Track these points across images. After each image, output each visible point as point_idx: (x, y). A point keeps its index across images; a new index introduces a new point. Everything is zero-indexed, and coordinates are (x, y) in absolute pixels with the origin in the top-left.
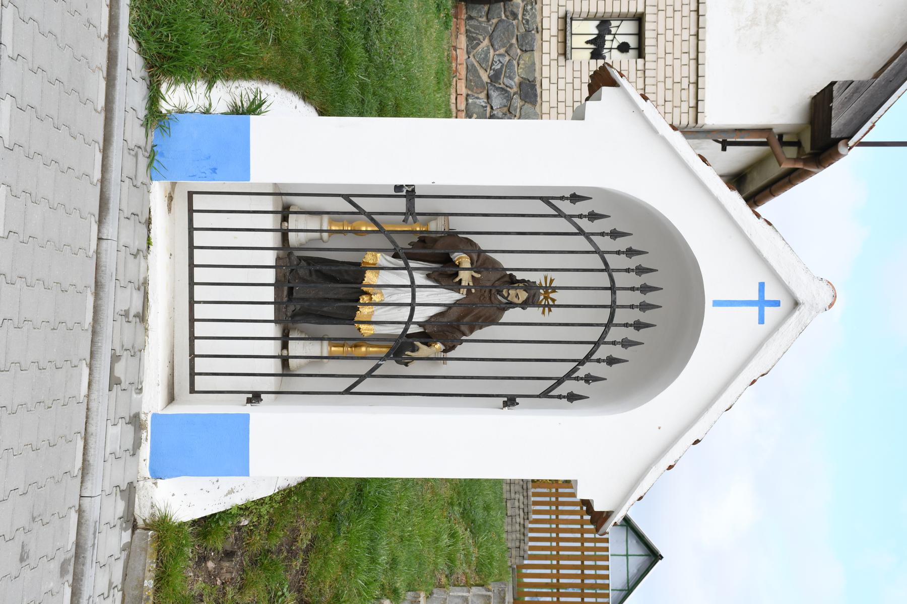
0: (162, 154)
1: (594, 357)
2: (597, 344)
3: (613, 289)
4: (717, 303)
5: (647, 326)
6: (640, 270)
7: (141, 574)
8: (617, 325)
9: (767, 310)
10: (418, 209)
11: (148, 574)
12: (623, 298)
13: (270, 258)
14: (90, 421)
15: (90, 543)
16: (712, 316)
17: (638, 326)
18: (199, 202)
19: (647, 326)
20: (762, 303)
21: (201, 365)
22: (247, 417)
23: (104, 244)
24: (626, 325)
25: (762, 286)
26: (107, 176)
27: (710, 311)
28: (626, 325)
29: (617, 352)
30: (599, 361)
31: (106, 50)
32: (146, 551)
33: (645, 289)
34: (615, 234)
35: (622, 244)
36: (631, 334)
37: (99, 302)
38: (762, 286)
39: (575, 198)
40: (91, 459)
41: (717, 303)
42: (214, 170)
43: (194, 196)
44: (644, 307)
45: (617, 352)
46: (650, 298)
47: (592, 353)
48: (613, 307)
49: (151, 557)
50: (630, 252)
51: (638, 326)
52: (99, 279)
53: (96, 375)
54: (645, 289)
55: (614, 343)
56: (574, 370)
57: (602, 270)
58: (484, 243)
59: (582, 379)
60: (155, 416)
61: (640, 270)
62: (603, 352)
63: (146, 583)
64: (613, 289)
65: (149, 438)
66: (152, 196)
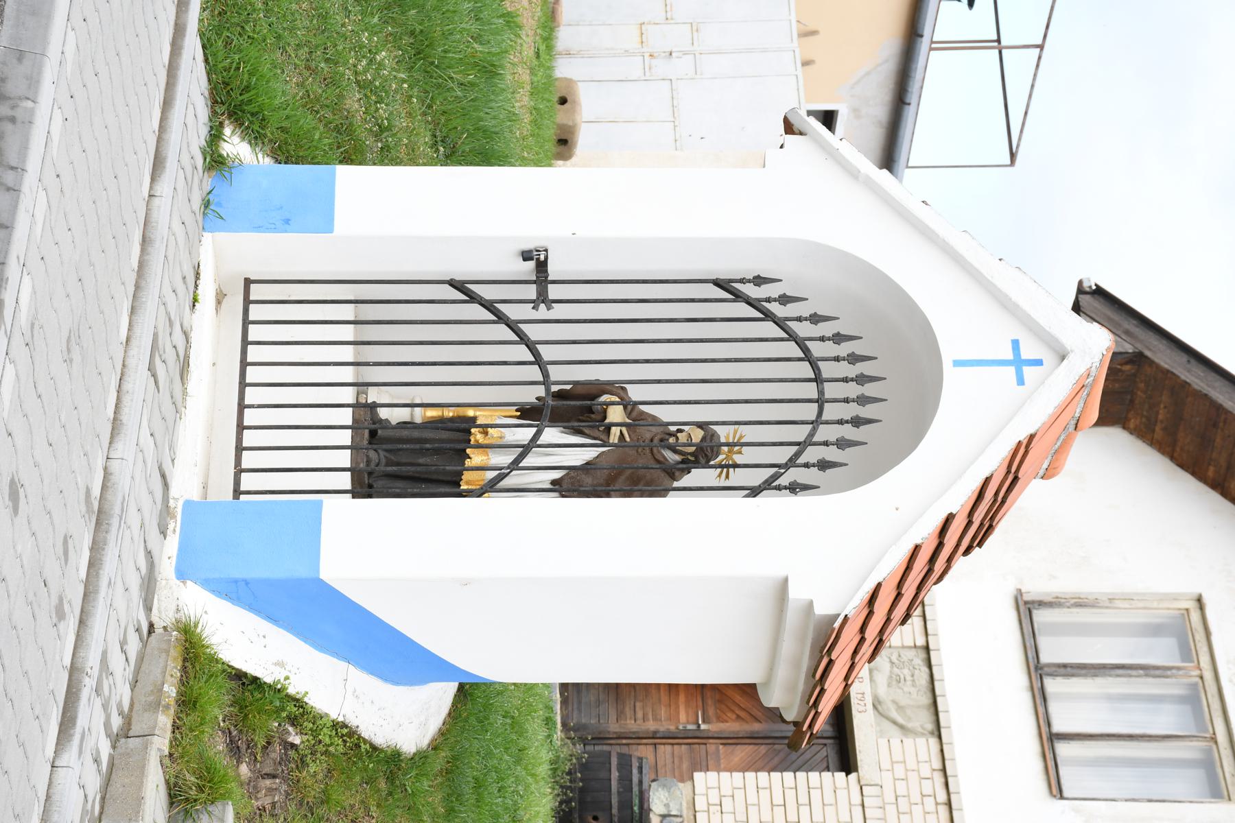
0: (219, 204)
1: (801, 460)
2: (802, 446)
3: (818, 379)
4: (957, 363)
5: (869, 421)
6: (854, 359)
7: (160, 677)
8: (827, 423)
9: (1028, 371)
10: (552, 296)
11: (168, 677)
12: (831, 390)
13: (346, 417)
14: (126, 378)
15: (117, 510)
16: (953, 381)
17: (857, 422)
18: (257, 292)
19: (869, 421)
20: (1018, 363)
21: (248, 481)
22: (321, 502)
23: (156, 201)
24: (841, 422)
25: (1016, 344)
26: (165, 136)
27: (950, 375)
28: (841, 422)
29: (832, 454)
30: (807, 465)
31: (172, 23)
32: (167, 652)
33: (861, 379)
34: (815, 319)
35: (826, 329)
36: (848, 432)
37: (146, 258)
38: (1016, 344)
39: (759, 281)
40: (125, 417)
41: (957, 363)
42: (287, 221)
43: (252, 286)
44: (863, 400)
45: (832, 454)
46: (869, 390)
47: (797, 455)
48: (821, 401)
49: (175, 659)
50: (838, 338)
51: (857, 422)
52: (147, 234)
53: (137, 331)
54: (861, 379)
55: (826, 444)
56: (776, 477)
57: (800, 359)
58: (635, 393)
59: (785, 488)
60: (188, 504)
61: (854, 359)
62: (811, 455)
63: (166, 688)
64: (818, 379)
65: (178, 530)
66: (202, 250)
